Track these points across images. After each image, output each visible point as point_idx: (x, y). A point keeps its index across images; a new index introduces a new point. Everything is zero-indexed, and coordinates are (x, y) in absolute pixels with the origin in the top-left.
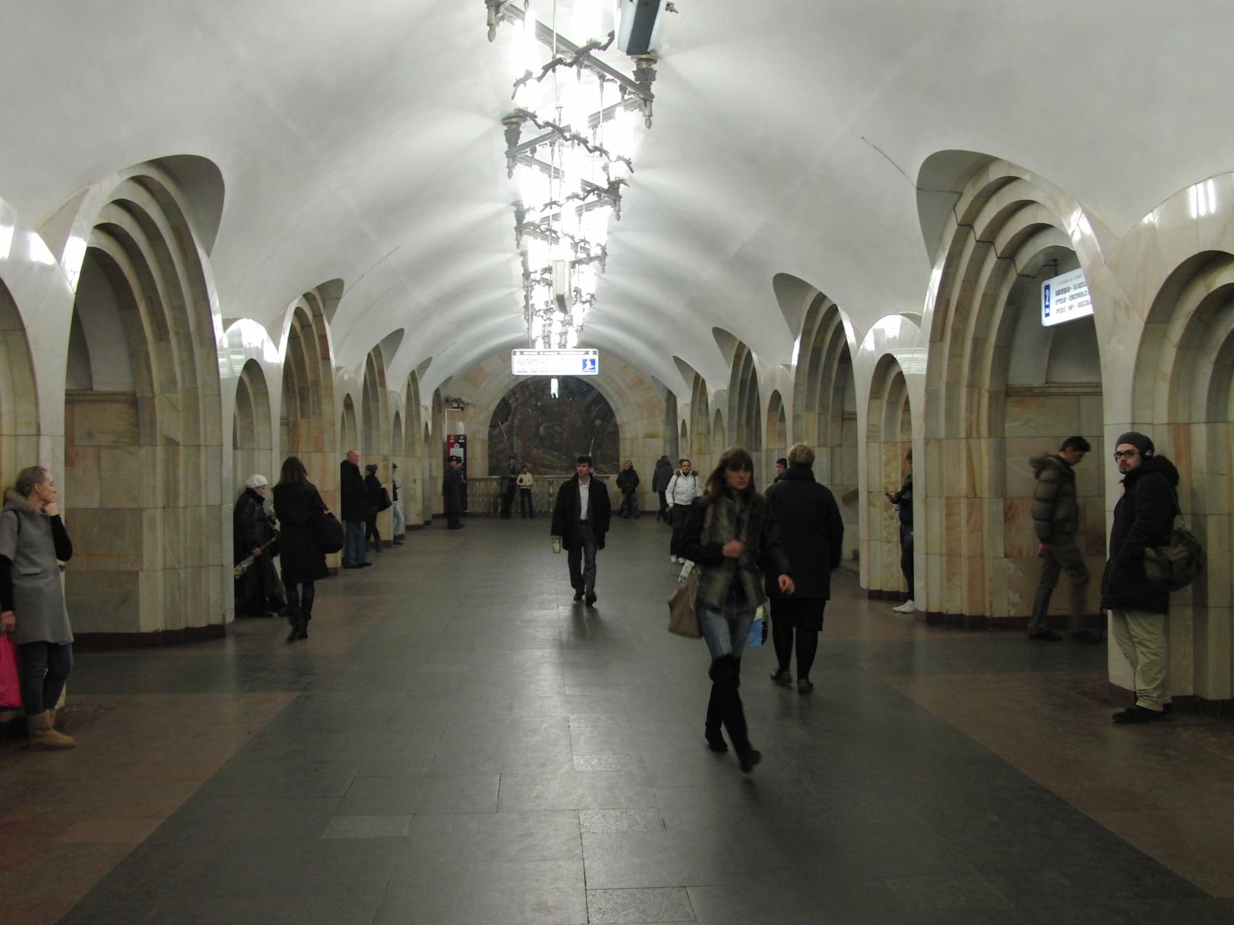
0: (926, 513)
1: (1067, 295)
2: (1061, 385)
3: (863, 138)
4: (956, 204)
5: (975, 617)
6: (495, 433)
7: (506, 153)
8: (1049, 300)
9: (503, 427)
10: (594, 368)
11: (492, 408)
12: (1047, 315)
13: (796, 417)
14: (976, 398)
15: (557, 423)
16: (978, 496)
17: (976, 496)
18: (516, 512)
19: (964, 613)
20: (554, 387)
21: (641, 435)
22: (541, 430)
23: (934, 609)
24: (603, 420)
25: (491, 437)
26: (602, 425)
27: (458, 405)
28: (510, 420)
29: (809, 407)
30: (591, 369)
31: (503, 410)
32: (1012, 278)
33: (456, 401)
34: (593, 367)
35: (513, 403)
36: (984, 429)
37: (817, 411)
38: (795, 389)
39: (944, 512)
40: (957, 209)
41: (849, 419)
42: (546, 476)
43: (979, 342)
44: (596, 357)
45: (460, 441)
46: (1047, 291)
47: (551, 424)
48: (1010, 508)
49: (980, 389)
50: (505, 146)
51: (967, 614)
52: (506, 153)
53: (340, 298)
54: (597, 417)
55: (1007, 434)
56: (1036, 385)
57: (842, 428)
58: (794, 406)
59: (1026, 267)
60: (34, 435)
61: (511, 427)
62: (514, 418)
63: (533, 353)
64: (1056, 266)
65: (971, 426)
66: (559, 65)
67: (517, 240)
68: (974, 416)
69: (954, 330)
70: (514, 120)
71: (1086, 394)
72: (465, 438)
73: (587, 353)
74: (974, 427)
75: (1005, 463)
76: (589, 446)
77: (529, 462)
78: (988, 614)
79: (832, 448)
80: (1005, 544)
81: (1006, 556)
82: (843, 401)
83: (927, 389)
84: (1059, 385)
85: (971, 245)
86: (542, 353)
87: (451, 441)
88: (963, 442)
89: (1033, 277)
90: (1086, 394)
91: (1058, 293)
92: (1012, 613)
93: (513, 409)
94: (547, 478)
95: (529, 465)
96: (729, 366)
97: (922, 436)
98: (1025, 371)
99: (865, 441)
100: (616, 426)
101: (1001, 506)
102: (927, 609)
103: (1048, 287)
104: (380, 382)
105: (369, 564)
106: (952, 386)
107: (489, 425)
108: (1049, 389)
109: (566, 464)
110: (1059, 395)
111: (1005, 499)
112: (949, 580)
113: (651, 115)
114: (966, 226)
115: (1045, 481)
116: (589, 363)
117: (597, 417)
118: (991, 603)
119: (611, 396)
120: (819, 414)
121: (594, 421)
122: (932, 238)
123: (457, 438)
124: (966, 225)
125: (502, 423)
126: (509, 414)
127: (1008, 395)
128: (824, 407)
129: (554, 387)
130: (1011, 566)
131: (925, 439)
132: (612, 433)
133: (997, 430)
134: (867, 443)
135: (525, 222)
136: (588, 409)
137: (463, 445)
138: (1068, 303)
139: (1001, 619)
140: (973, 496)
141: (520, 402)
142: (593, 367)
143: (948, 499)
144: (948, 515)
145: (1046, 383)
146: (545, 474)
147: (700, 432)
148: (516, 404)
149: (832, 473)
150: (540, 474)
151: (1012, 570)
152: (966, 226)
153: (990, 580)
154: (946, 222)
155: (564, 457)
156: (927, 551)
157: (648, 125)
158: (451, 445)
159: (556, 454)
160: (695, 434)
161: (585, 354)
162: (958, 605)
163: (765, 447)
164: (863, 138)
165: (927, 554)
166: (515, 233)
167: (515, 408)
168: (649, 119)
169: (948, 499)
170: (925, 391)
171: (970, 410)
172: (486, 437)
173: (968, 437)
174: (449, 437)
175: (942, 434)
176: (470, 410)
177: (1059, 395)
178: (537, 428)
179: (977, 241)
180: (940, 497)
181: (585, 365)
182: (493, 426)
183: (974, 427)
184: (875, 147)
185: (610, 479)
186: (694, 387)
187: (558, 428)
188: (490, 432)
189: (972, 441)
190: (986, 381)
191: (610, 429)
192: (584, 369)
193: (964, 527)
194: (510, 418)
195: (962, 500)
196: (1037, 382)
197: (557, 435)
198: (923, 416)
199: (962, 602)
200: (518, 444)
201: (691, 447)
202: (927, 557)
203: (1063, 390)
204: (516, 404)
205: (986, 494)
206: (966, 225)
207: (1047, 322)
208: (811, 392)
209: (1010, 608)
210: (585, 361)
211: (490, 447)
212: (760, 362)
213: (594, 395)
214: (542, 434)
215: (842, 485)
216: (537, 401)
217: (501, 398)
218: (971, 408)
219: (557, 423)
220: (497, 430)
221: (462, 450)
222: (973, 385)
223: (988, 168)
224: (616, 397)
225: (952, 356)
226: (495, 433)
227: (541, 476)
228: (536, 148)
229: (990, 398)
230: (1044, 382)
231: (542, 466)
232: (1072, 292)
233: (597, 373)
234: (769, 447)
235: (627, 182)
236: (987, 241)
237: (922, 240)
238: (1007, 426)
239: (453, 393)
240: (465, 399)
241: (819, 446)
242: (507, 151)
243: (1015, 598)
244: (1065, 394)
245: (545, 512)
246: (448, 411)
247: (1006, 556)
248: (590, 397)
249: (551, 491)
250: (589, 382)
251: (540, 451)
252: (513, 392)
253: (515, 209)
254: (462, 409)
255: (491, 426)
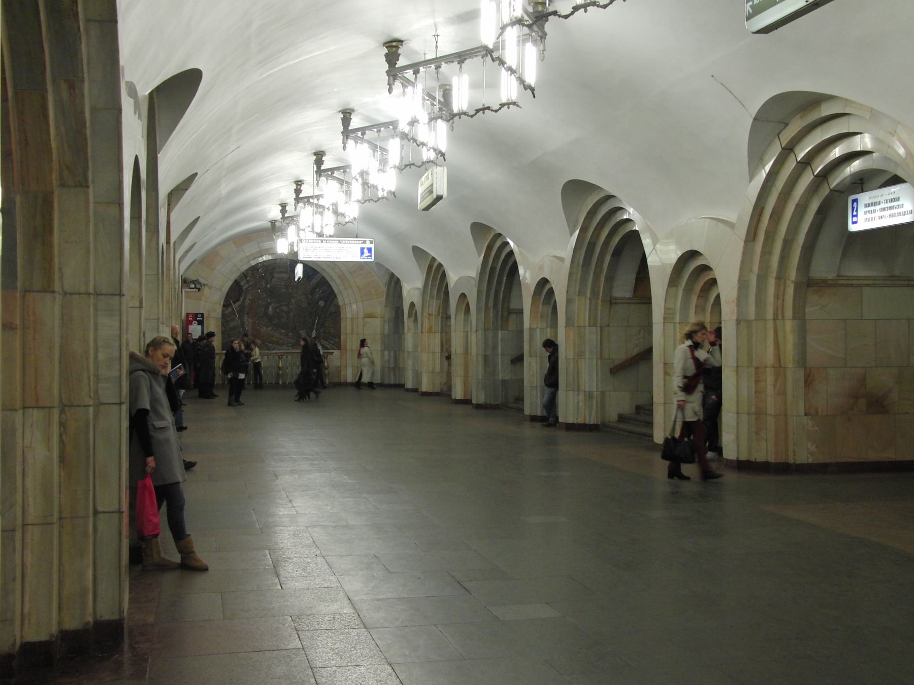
0: (737, 380)
1: (878, 207)
2: (849, 278)
3: (712, 76)
4: (780, 132)
5: (780, 464)
6: (227, 312)
7: (386, 72)
8: (857, 211)
9: (235, 306)
10: (371, 256)
11: (226, 289)
12: (854, 223)
13: (569, 301)
14: (782, 287)
15: (284, 304)
16: (783, 365)
17: (781, 366)
18: (249, 384)
19: (769, 461)
20: (299, 271)
21: (361, 315)
22: (270, 309)
23: (743, 457)
24: (326, 301)
25: (224, 315)
26: (325, 306)
27: (195, 286)
28: (241, 300)
29: (581, 293)
30: (367, 256)
31: (236, 291)
32: (824, 192)
33: (193, 282)
34: (370, 254)
35: (244, 285)
36: (789, 313)
37: (588, 295)
38: (569, 277)
39: (753, 379)
40: (780, 136)
41: (616, 303)
42: (274, 351)
43: (788, 243)
44: (372, 246)
45: (198, 319)
46: (855, 204)
47: (278, 304)
48: (809, 376)
49: (785, 280)
50: (386, 67)
51: (774, 462)
52: (386, 72)
53: (187, 190)
54: (321, 299)
55: (807, 317)
56: (830, 278)
57: (610, 311)
58: (567, 292)
59: (838, 185)
60: (137, 307)
61: (242, 307)
62: (245, 298)
63: (332, 242)
64: (862, 184)
65: (777, 310)
66: (553, 16)
67: (343, 143)
68: (780, 302)
69: (767, 233)
70: (394, 44)
71: (868, 285)
72: (202, 315)
73: (364, 242)
74: (780, 310)
75: (806, 340)
76: (313, 324)
77: (258, 338)
78: (791, 461)
79: (601, 328)
80: (805, 403)
81: (806, 415)
82: (612, 287)
83: (739, 280)
84: (847, 278)
85: (790, 166)
86: (325, 241)
87: (190, 319)
88: (770, 325)
89: (842, 192)
90: (868, 285)
91: (867, 205)
92: (810, 460)
93: (244, 289)
94: (277, 353)
95: (259, 342)
96: (479, 256)
97: (734, 317)
98: (822, 269)
99: (662, 321)
100: (338, 307)
101: (802, 373)
102: (737, 458)
103: (855, 201)
104: (504, 298)
105: (186, 428)
106: (762, 278)
107: (222, 304)
108: (840, 281)
109: (293, 341)
110: (847, 286)
111: (805, 368)
112: (757, 433)
113: (544, 50)
114: (789, 150)
115: (696, 360)
116: (366, 251)
117: (321, 299)
118: (794, 452)
119: (332, 278)
120: (590, 299)
121: (317, 302)
122: (755, 159)
123: (195, 316)
124: (788, 149)
125: (234, 303)
126: (240, 296)
127: (808, 286)
128: (595, 293)
129: (299, 271)
130: (810, 422)
131: (737, 320)
132: (334, 313)
133: (799, 314)
134: (664, 323)
135: (350, 128)
136: (313, 292)
137: (201, 323)
138: (878, 214)
139: (802, 465)
140: (779, 367)
141: (251, 284)
142: (370, 254)
143: (757, 368)
144: (757, 381)
145: (838, 276)
146: (273, 349)
147: (430, 312)
148: (247, 285)
149: (601, 349)
150: (269, 350)
151: (810, 425)
152: (789, 150)
153: (794, 433)
154: (770, 144)
155: (290, 334)
156: (738, 411)
157: (542, 58)
158: (190, 323)
159: (284, 331)
160: (425, 314)
161: (362, 243)
162: (764, 453)
163: (529, 327)
164: (712, 76)
165: (737, 413)
166: (342, 137)
167: (247, 289)
168: (543, 53)
169: (757, 368)
170: (738, 281)
171: (777, 297)
172: (220, 316)
173: (775, 318)
174: (188, 315)
175: (752, 315)
176: (206, 291)
177: (847, 286)
178: (267, 307)
179: (798, 162)
180: (748, 367)
181: (362, 253)
182: (226, 305)
183: (780, 310)
184: (722, 84)
185: (334, 354)
186: (427, 273)
187: (285, 308)
188: (223, 311)
189: (778, 322)
190: (793, 274)
191: (332, 309)
192: (361, 256)
193: (770, 390)
194: (242, 298)
195: (768, 369)
196: (831, 276)
197: (284, 315)
198: (736, 301)
199: (767, 451)
200: (248, 322)
201: (422, 325)
202: (738, 417)
203: (849, 282)
204: (247, 285)
205: (791, 365)
206: (788, 149)
207: (853, 228)
208: (583, 280)
209: (809, 456)
210: (362, 250)
211: (223, 325)
212: (521, 253)
213: (319, 279)
214: (270, 313)
215: (609, 359)
216: (267, 283)
217: (234, 280)
218: (778, 295)
219: (284, 304)
220: (230, 309)
221: (200, 327)
222: (781, 278)
223: (820, 104)
224: (338, 281)
225: (763, 254)
226: (228, 312)
227: (270, 352)
228: (419, 70)
229: (795, 289)
230: (836, 275)
231: (269, 343)
232: (883, 206)
233: (372, 260)
234: (531, 327)
235: (520, 104)
236: (807, 162)
237: (746, 160)
238: (807, 310)
239: (191, 276)
240: (201, 280)
241: (589, 326)
242: (388, 70)
243: (813, 448)
244: (852, 286)
245: (275, 383)
246: (185, 291)
247: (806, 415)
248: (314, 281)
249: (280, 365)
250: (315, 267)
251: (269, 329)
252: (244, 275)
253: (342, 116)
254: (199, 289)
255: (224, 306)
